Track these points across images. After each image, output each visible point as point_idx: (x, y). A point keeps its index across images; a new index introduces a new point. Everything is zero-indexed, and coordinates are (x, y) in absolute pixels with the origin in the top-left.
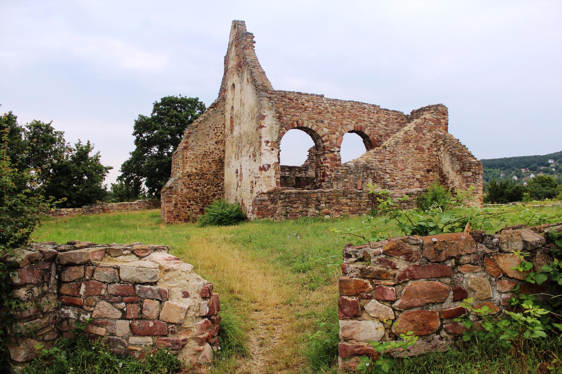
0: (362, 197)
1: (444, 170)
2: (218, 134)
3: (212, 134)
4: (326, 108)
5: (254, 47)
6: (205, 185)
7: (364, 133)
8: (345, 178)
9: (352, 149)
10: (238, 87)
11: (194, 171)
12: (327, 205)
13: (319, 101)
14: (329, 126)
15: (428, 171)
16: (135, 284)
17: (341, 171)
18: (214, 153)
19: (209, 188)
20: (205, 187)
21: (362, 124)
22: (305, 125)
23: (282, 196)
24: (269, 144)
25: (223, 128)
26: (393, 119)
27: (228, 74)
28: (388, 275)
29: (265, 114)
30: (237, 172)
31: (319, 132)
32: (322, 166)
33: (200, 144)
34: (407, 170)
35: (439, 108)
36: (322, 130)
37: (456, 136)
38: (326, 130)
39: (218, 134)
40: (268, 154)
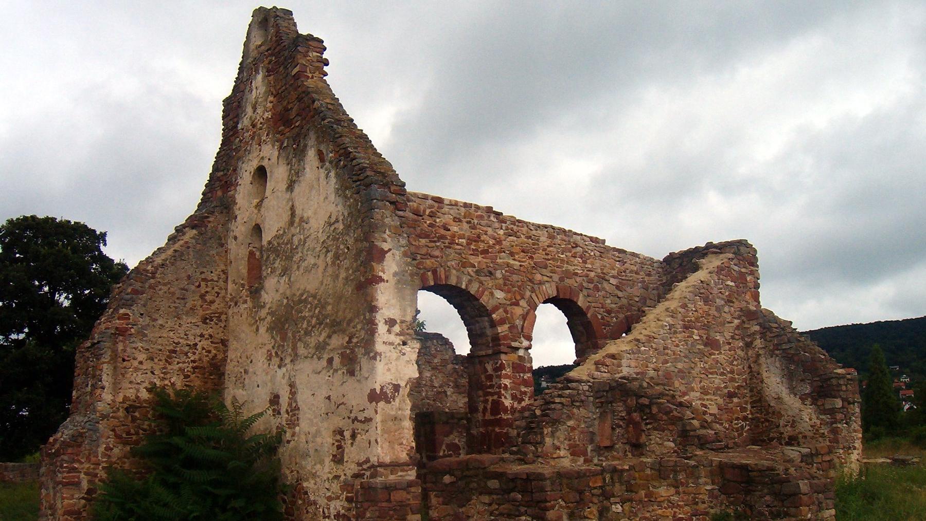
0: (698, 478)
2: (208, 298)
3: (193, 300)
4: (499, 242)
5: (326, 74)
7: (576, 303)
8: (569, 418)
9: (551, 342)
10: (279, 174)
12: (627, 506)
13: (483, 223)
15: (731, 395)
17: (557, 400)
22: (453, 281)
23: (493, 484)
24: (397, 329)
25: (221, 283)
26: (631, 272)
29: (385, 246)
30: (275, 400)
31: (484, 300)
32: (492, 386)
33: (160, 322)
34: (692, 394)
35: (742, 249)
36: (492, 294)
38: (499, 294)
40: (394, 355)
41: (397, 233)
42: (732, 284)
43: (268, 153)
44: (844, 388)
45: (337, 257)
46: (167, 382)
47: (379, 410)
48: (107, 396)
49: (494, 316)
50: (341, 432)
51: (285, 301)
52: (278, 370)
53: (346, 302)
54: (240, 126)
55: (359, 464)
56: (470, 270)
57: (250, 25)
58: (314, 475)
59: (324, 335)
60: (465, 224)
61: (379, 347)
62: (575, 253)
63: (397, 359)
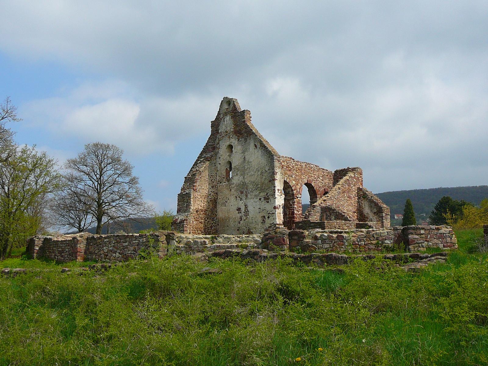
1: (364, 212)
2: (213, 181)
4: (293, 167)
6: (206, 219)
10: (238, 148)
11: (200, 208)
13: (290, 162)
17: (312, 211)
18: (211, 195)
19: (209, 221)
20: (206, 220)
24: (280, 191)
30: (239, 209)
31: (290, 184)
36: (292, 182)
38: (294, 182)
39: (213, 181)
40: (279, 198)
42: (355, 180)
43: (234, 141)
44: (386, 210)
45: (262, 173)
46: (204, 204)
47: (276, 211)
48: (192, 208)
49: (293, 188)
50: (264, 217)
51: (242, 183)
52: (240, 201)
53: (265, 185)
54: (220, 131)
55: (270, 224)
56: (287, 175)
57: (222, 101)
59: (258, 193)
60: (285, 162)
61: (276, 196)
62: (312, 170)
63: (280, 199)
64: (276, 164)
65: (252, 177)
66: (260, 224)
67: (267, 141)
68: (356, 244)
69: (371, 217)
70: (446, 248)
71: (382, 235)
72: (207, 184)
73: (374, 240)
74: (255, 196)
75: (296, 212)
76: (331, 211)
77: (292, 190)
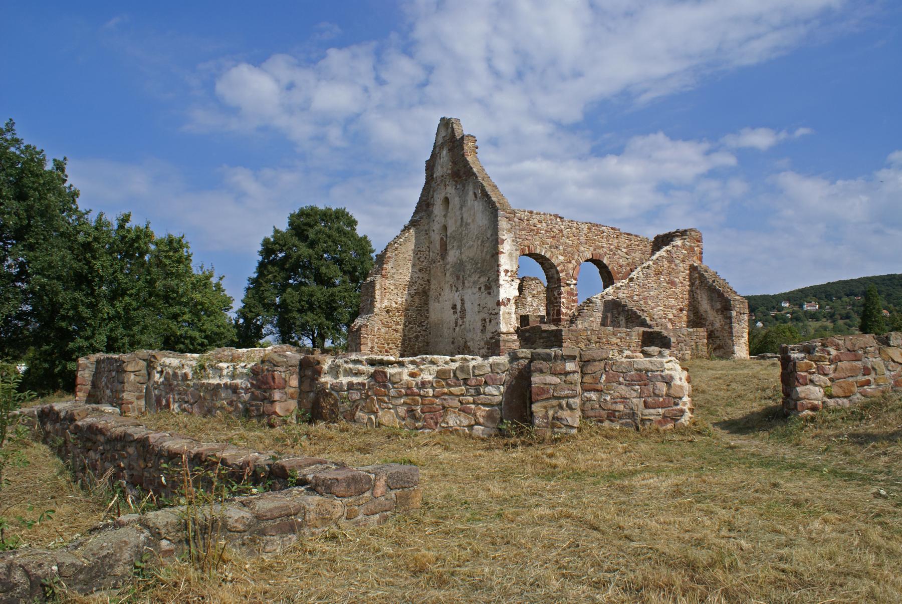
2: (422, 259)
4: (561, 231)
10: (455, 201)
11: (394, 305)
14: (564, 253)
16: (647, 371)
19: (412, 328)
21: (600, 251)
23: (544, 335)
24: (509, 274)
27: (433, 184)
28: (825, 358)
29: (504, 238)
30: (454, 307)
31: (553, 260)
37: (712, 269)
38: (561, 258)
39: (422, 259)
40: (508, 285)
41: (509, 231)
43: (450, 190)
45: (483, 242)
48: (378, 305)
50: (485, 320)
58: (473, 339)
61: (501, 282)
64: (503, 224)
65: (471, 251)
66: (479, 334)
67: (495, 187)
68: (413, 394)
69: (712, 318)
70: (652, 411)
71: (477, 372)
72: (410, 265)
73: (456, 386)
74: (474, 283)
75: (564, 310)
76: (621, 309)
77: (558, 272)
